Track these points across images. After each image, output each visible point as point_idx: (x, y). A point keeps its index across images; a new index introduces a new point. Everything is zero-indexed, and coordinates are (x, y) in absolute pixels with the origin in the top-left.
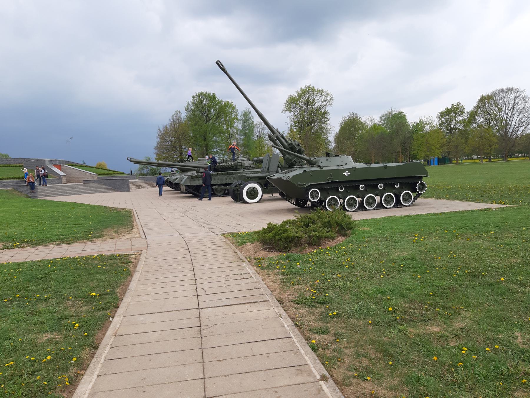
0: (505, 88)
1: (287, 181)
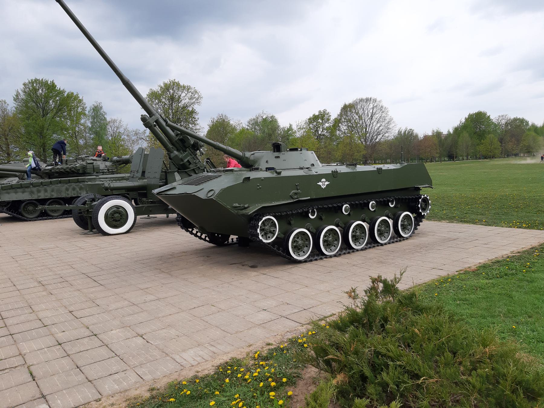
0: (364, 97)
1: (209, 202)
